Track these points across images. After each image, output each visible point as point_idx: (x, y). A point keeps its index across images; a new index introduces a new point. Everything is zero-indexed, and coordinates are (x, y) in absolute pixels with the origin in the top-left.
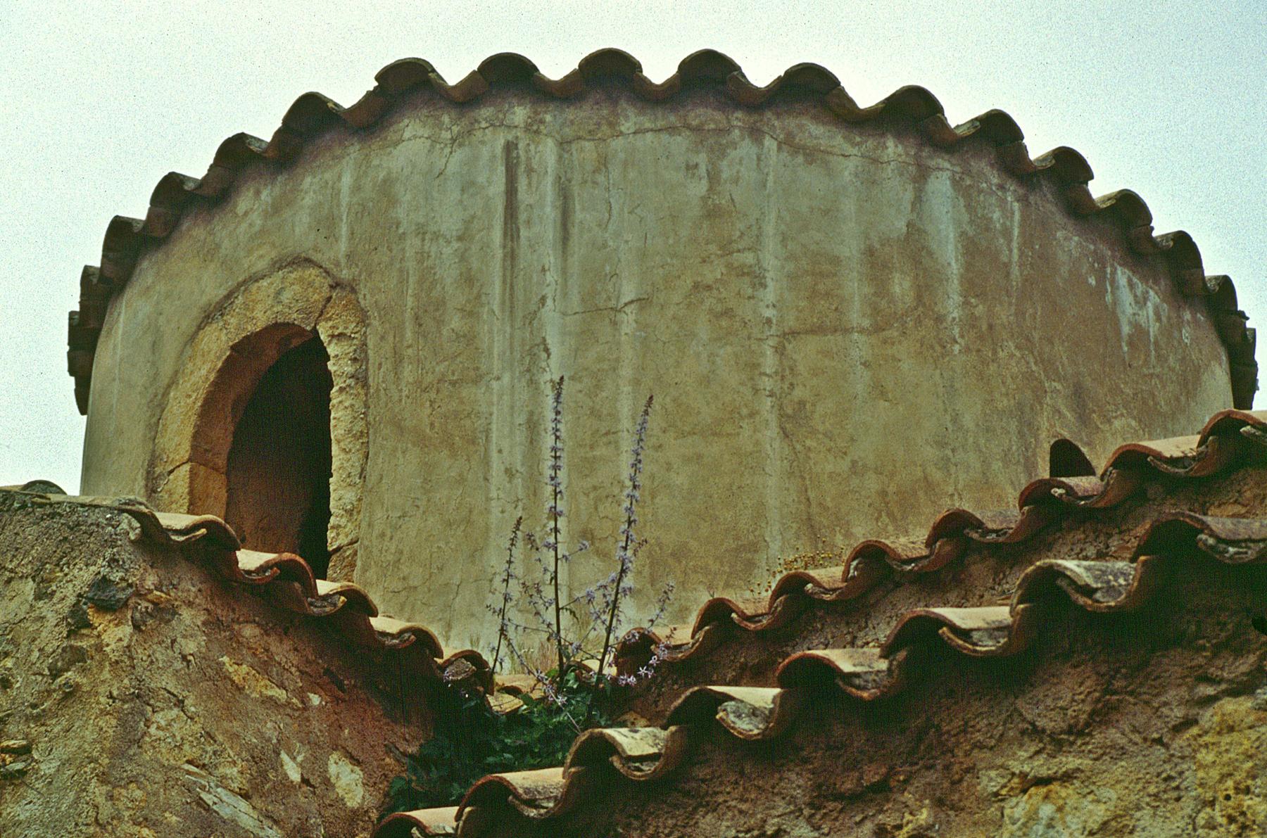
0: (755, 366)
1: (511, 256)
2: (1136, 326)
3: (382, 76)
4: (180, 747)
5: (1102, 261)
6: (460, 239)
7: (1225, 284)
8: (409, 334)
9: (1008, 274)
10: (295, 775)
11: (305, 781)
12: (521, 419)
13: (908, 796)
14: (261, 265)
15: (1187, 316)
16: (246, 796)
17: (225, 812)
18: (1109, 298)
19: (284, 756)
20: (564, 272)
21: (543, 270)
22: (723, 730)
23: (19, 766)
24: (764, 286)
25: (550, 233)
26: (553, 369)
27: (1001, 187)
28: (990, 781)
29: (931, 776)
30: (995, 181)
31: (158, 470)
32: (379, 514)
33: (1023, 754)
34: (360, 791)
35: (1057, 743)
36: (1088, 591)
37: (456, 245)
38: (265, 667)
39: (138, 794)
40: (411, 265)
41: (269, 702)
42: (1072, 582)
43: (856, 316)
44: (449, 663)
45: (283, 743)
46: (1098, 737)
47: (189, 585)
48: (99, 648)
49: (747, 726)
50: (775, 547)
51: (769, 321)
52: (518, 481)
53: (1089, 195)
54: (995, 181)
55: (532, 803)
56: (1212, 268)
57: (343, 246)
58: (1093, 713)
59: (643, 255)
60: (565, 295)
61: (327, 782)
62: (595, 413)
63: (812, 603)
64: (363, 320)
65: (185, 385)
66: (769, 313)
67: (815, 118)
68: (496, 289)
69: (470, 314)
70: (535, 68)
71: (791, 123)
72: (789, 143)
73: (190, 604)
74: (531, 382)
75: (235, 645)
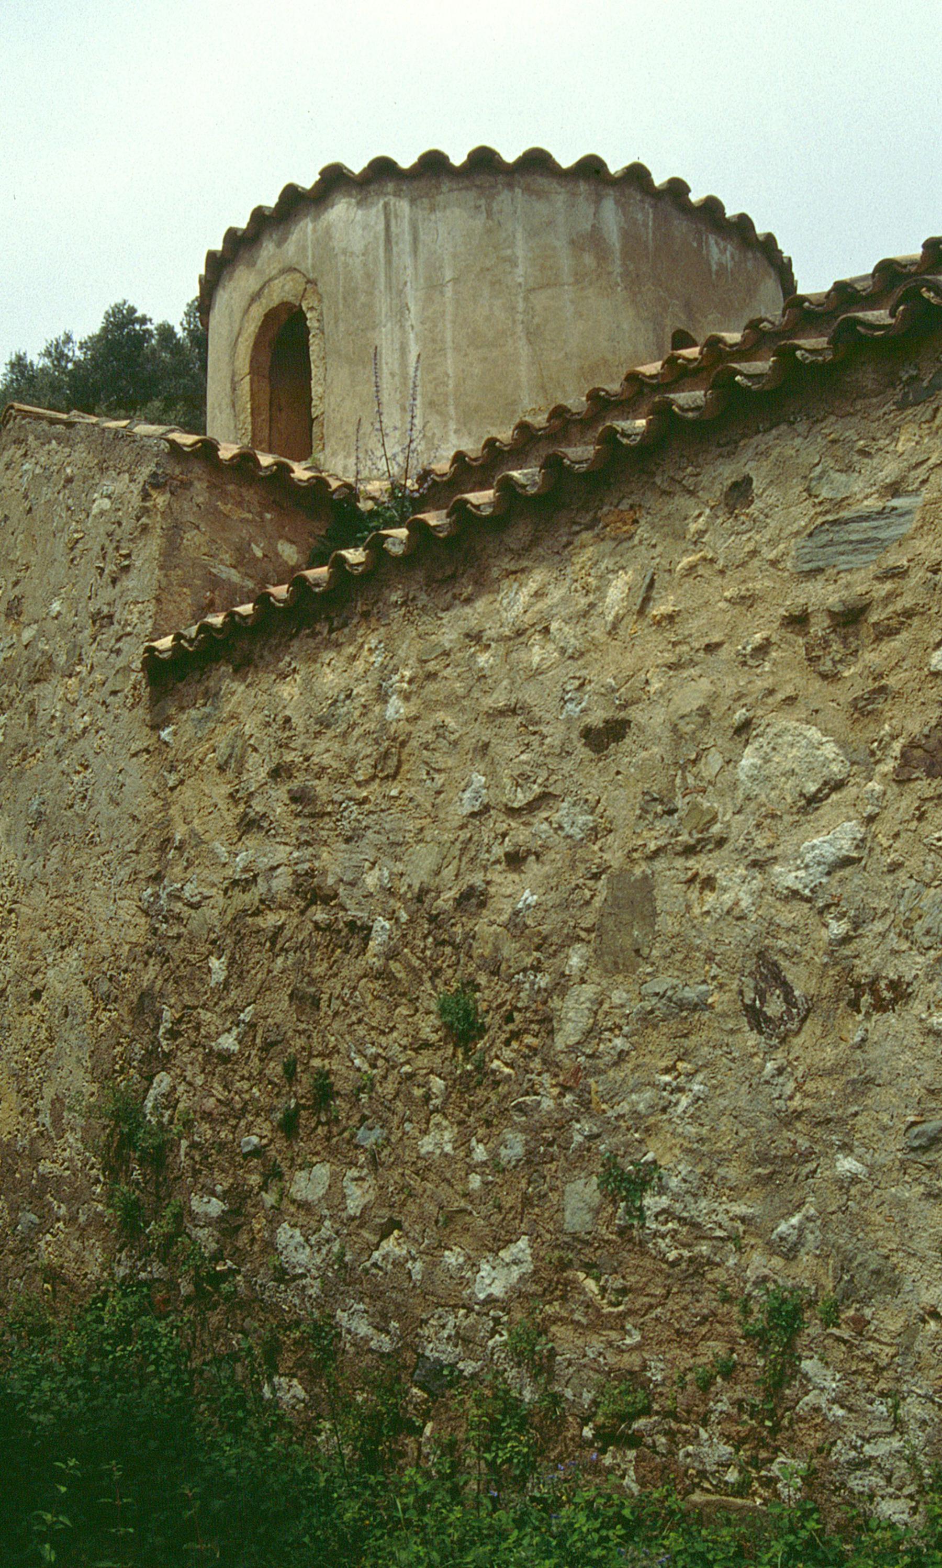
0: (513, 308)
1: (389, 262)
2: (720, 264)
3: (322, 173)
4: (199, 548)
5: (699, 232)
6: (363, 255)
7: (770, 238)
8: (341, 306)
9: (647, 247)
10: (259, 554)
11: (265, 556)
12: (397, 346)
13: (464, 580)
14: (274, 272)
15: (750, 255)
16: (235, 567)
17: (224, 576)
18: (704, 252)
19: (253, 546)
20: (416, 268)
21: (405, 268)
22: (386, 551)
23: (126, 563)
24: (517, 266)
25: (408, 248)
26: (413, 317)
27: (642, 201)
28: (495, 573)
29: (473, 571)
30: (639, 198)
31: (236, 379)
32: (332, 399)
33: (507, 560)
34: (296, 557)
35: (518, 555)
36: (524, 486)
37: (361, 258)
38: (239, 504)
39: (180, 572)
40: (341, 269)
41: (242, 520)
42: (516, 483)
43: (567, 277)
44: (336, 490)
45: (252, 539)
46: (534, 552)
47: (198, 469)
48: (155, 506)
49: (397, 550)
50: (526, 401)
51: (520, 284)
52: (397, 378)
53: (689, 201)
54: (639, 198)
55: (318, 585)
56: (760, 229)
57: (310, 261)
58: (531, 541)
59: (455, 256)
60: (416, 279)
61: (278, 555)
62: (434, 341)
63: (500, 451)
64: (320, 301)
65: (245, 335)
66: (520, 280)
67: (542, 175)
68: (382, 279)
69: (370, 294)
70: (395, 164)
71: (529, 179)
72: (527, 190)
73: (199, 479)
74: (402, 327)
75: (224, 495)
